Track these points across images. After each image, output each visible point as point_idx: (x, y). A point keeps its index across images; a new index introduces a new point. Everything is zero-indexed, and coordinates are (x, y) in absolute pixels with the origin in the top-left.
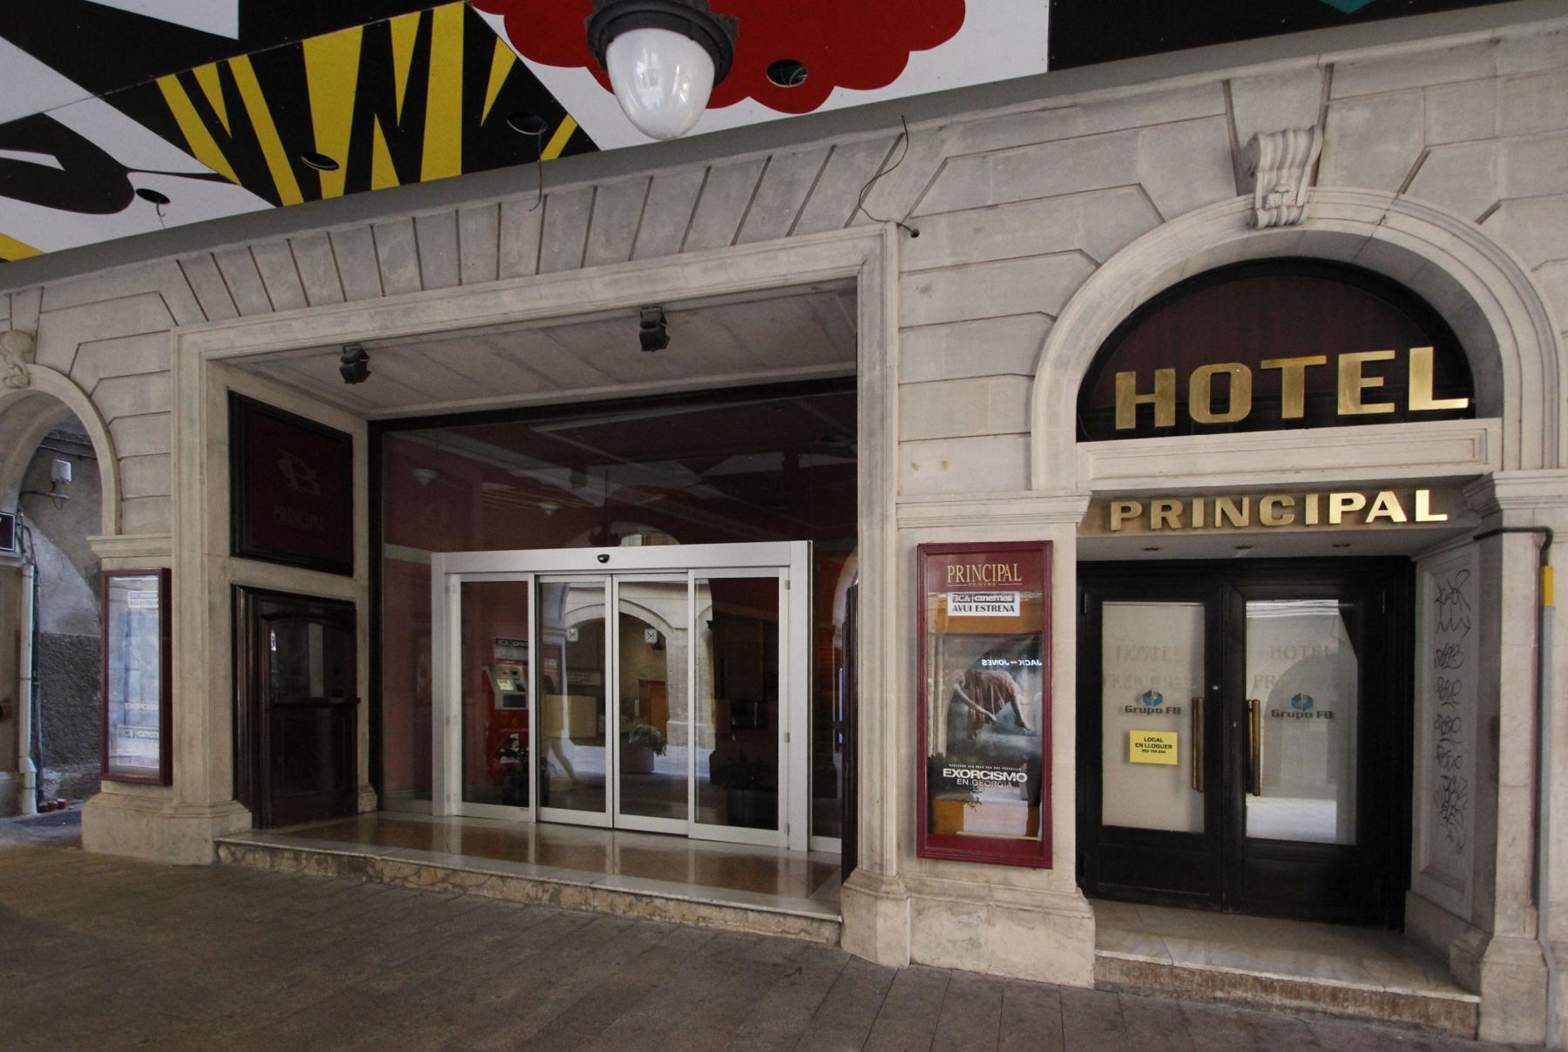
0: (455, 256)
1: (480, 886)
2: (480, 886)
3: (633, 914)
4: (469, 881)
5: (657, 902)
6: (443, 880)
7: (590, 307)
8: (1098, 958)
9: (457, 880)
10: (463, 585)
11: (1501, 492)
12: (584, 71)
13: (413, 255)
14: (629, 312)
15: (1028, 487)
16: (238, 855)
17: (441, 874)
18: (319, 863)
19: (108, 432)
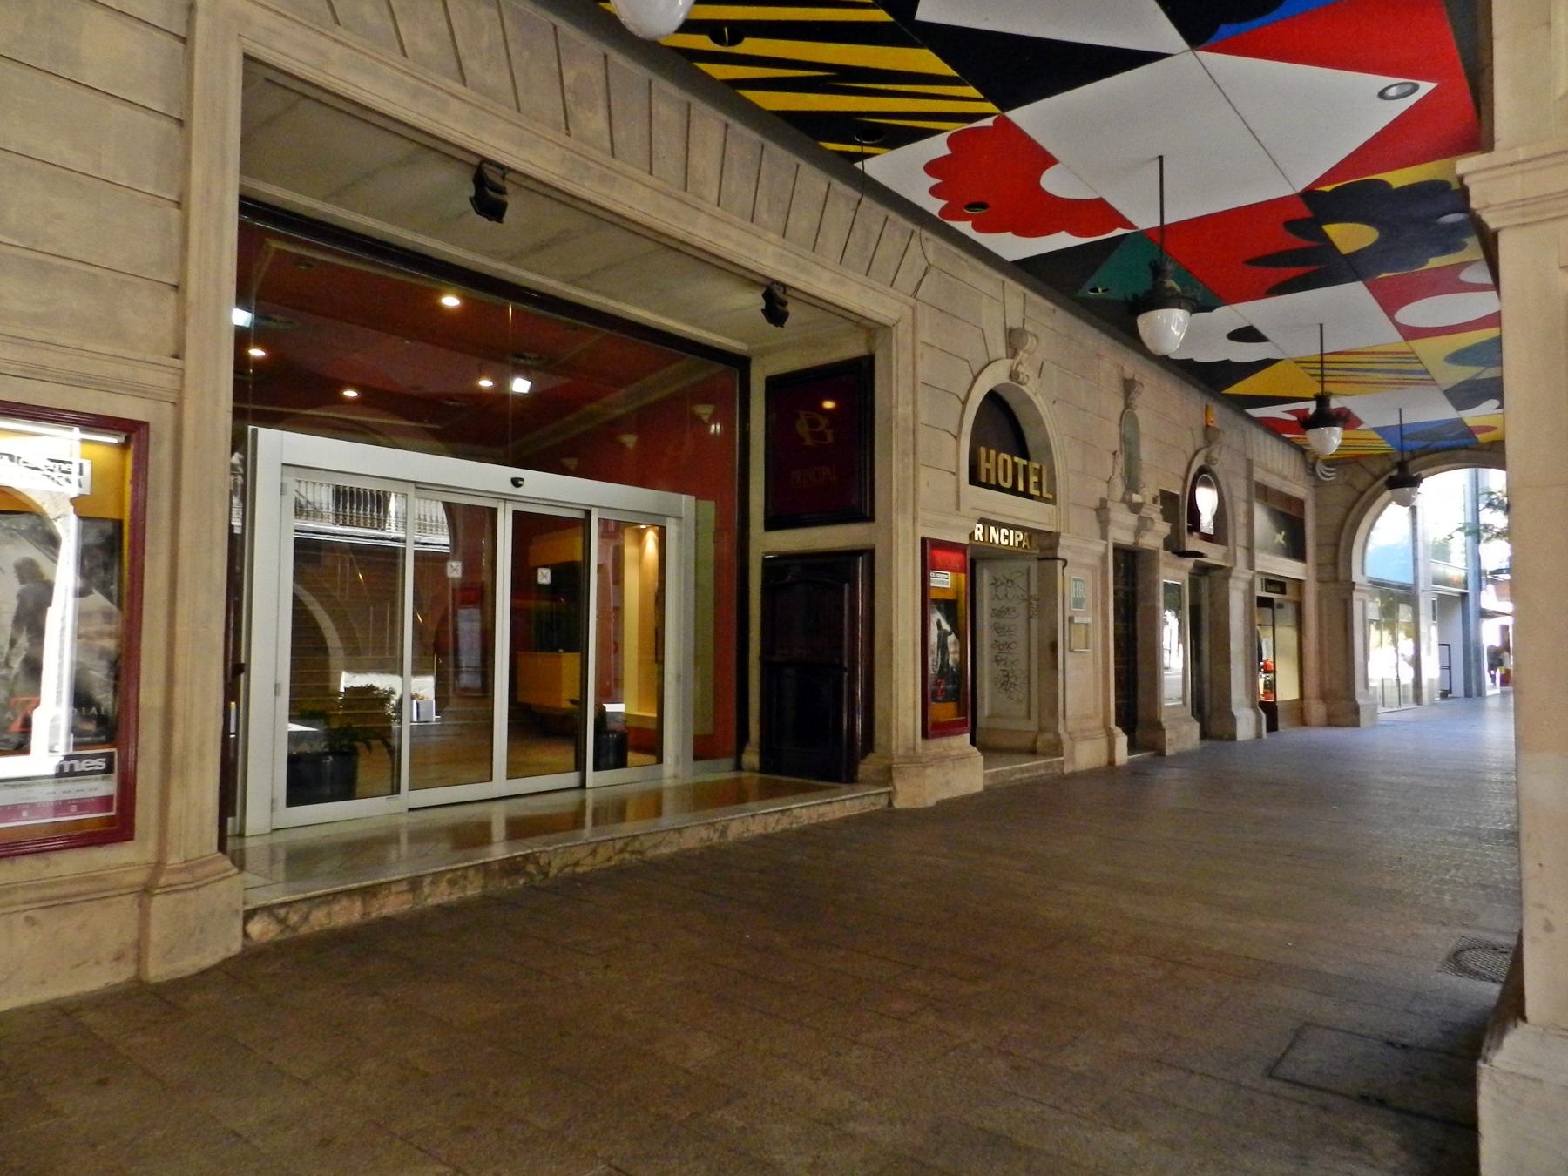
0: (645, 133)
1: (656, 846)
2: (656, 846)
3: (780, 827)
4: (648, 842)
5: (796, 812)
6: (622, 851)
7: (752, 266)
8: (1500, 363)
9: (636, 845)
10: (516, 514)
11: (1062, 541)
12: (1010, 259)
13: (601, 103)
14: (760, 279)
15: (958, 509)
16: (294, 918)
17: (619, 845)
18: (452, 883)
19: (1339, 538)
